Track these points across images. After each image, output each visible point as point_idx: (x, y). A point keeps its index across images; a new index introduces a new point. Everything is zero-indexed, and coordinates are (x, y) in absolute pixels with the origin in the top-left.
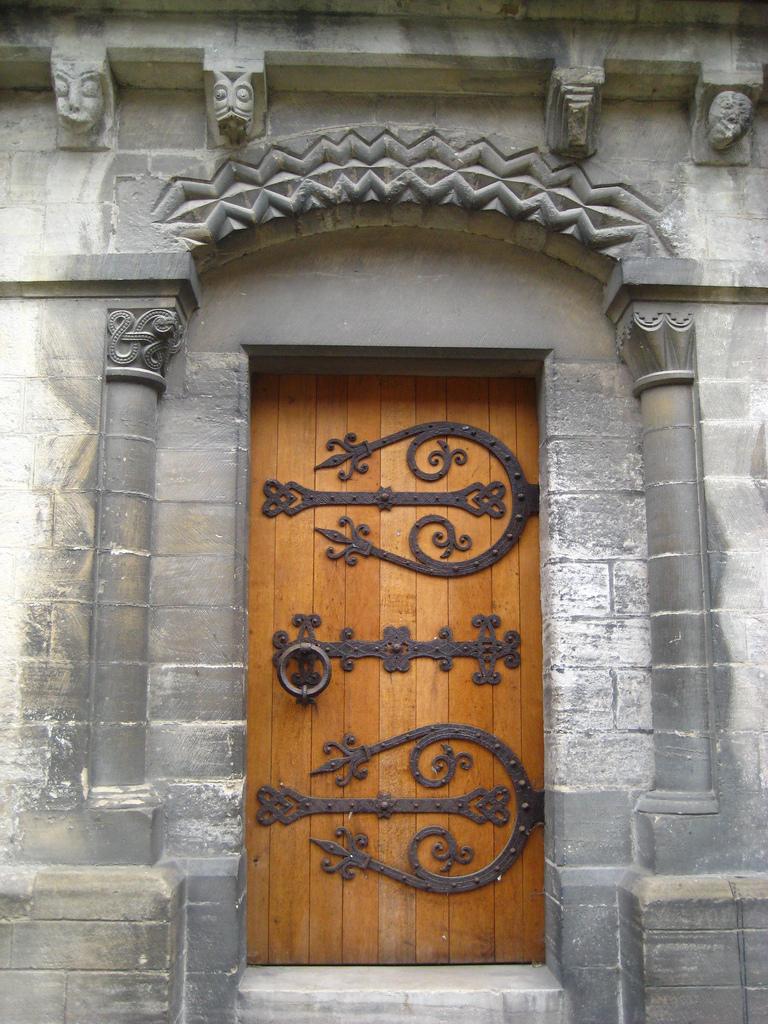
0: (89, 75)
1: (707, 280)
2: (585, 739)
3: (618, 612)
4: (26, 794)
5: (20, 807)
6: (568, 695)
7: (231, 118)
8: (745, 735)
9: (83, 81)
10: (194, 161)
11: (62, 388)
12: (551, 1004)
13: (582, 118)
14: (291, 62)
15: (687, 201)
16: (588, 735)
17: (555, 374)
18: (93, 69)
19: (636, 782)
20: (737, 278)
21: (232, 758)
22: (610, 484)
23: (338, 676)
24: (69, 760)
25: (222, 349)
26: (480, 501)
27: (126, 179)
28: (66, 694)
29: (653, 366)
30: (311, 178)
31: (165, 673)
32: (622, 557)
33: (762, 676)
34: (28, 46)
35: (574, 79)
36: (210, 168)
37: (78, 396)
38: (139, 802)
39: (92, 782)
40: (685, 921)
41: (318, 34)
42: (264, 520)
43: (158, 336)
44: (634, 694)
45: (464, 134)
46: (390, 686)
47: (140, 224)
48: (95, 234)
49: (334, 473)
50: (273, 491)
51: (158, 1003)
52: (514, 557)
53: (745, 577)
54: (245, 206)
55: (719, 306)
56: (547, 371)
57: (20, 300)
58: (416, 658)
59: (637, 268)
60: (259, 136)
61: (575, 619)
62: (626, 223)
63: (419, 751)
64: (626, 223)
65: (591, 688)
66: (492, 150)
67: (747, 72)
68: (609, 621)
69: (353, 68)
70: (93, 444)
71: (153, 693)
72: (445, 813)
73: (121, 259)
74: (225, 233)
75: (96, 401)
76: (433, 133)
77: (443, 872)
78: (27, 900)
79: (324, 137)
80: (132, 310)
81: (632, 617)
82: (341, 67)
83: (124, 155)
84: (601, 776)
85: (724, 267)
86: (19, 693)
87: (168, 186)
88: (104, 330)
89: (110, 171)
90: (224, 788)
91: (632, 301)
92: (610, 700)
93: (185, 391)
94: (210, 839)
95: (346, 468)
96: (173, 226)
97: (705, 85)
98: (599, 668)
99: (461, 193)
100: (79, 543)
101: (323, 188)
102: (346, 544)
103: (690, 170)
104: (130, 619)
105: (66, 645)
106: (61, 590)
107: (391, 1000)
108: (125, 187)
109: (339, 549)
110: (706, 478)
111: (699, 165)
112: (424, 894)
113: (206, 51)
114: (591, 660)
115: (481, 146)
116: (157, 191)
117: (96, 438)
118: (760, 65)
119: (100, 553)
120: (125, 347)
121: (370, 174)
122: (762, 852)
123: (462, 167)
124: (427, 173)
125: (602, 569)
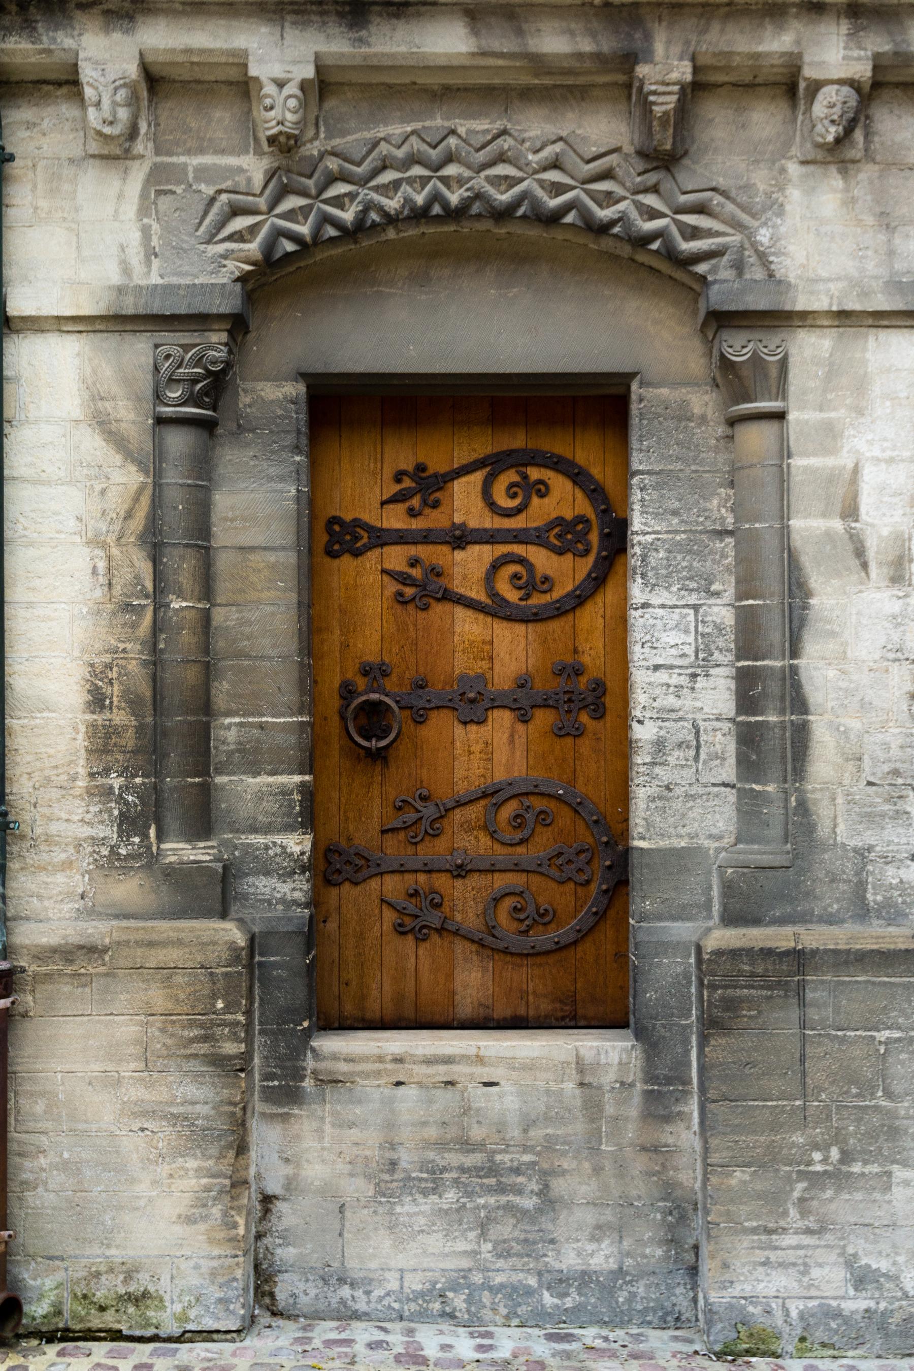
0: (122, 82)
1: (801, 305)
2: (666, 793)
3: (703, 660)
4: (94, 851)
5: (89, 864)
6: (648, 748)
7: (281, 133)
8: (821, 789)
9: (116, 89)
10: (240, 170)
11: (110, 433)
12: (624, 1056)
13: (668, 121)
14: (344, 62)
15: (788, 208)
16: (668, 788)
17: (641, 400)
18: (127, 75)
19: (719, 838)
20: (835, 301)
21: (301, 813)
22: (698, 523)
23: (409, 728)
24: (138, 817)
25: (277, 379)
26: (564, 536)
27: (165, 192)
28: (132, 752)
29: (748, 392)
30: (369, 189)
31: (229, 727)
32: (710, 602)
33: (842, 729)
34: (52, 47)
35: (659, 78)
36: (258, 179)
37: (129, 442)
38: (208, 858)
39: (160, 838)
40: (747, 968)
41: (373, 29)
42: (327, 560)
43: (209, 373)
44: (717, 746)
45: (539, 132)
46: (466, 737)
47: (184, 246)
48: (136, 257)
49: (401, 508)
50: (337, 528)
51: (235, 1045)
52: (599, 598)
53: (828, 627)
54: (298, 223)
55: (818, 330)
56: (634, 397)
57: (58, 333)
58: (493, 708)
59: (725, 288)
60: (311, 141)
61: (657, 668)
62: (718, 234)
63: (498, 806)
64: (718, 234)
65: (673, 740)
66: (571, 153)
67: (854, 62)
68: (692, 670)
69: (413, 67)
70: (148, 492)
71: (216, 748)
72: (523, 871)
73: (168, 290)
74: (278, 255)
75: (149, 446)
76: (504, 132)
77: (521, 933)
78: (105, 950)
79: (384, 139)
80: (181, 346)
81: (718, 666)
82: (401, 67)
83: (162, 163)
84: (683, 831)
85: (821, 288)
86: (83, 751)
87: (212, 200)
88: (151, 368)
89: (148, 182)
90: (292, 844)
91: (720, 327)
92: (692, 753)
93: (239, 426)
94: (279, 896)
95: (416, 502)
96: (221, 248)
97: (806, 79)
98: (681, 719)
99: (536, 204)
100: (137, 598)
101: (384, 201)
102: (416, 586)
103: (793, 169)
104: (192, 675)
105: (130, 703)
106: (121, 646)
107: (462, 1052)
108: (165, 203)
109: (409, 591)
110: (791, 522)
111: (804, 163)
112: (502, 956)
113: (250, 52)
114: (673, 711)
115: (558, 147)
116: (201, 207)
117: (150, 487)
118: (869, 53)
119: (159, 606)
120: (174, 386)
121: (435, 185)
122: (835, 906)
123: (536, 172)
124: (496, 181)
125: (687, 615)
